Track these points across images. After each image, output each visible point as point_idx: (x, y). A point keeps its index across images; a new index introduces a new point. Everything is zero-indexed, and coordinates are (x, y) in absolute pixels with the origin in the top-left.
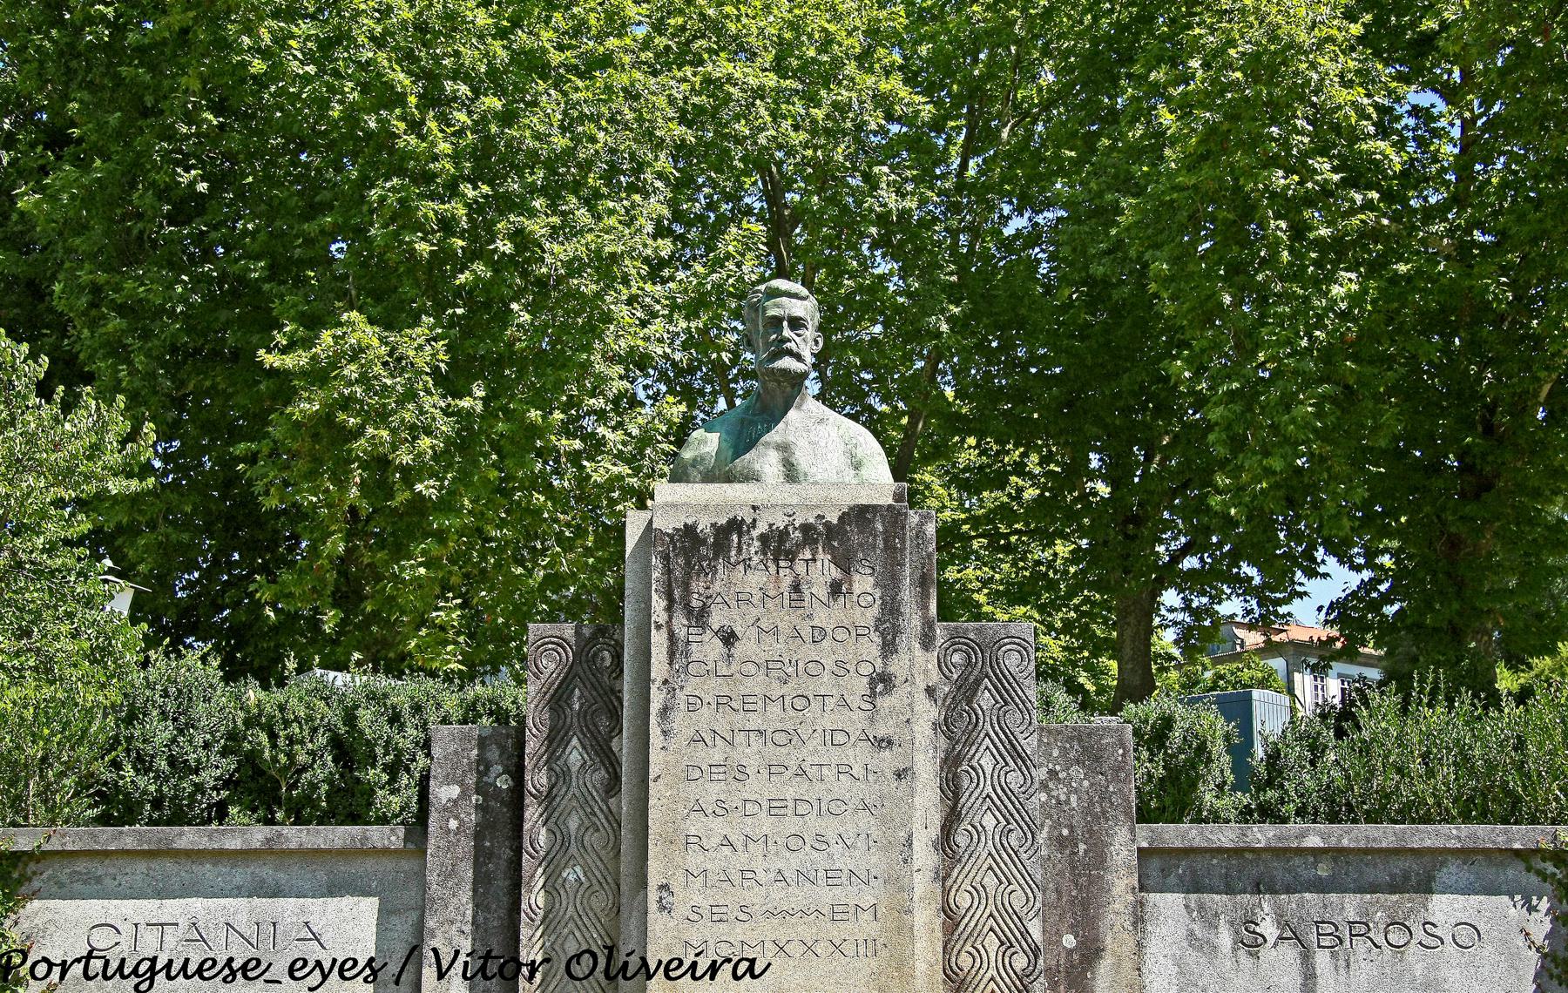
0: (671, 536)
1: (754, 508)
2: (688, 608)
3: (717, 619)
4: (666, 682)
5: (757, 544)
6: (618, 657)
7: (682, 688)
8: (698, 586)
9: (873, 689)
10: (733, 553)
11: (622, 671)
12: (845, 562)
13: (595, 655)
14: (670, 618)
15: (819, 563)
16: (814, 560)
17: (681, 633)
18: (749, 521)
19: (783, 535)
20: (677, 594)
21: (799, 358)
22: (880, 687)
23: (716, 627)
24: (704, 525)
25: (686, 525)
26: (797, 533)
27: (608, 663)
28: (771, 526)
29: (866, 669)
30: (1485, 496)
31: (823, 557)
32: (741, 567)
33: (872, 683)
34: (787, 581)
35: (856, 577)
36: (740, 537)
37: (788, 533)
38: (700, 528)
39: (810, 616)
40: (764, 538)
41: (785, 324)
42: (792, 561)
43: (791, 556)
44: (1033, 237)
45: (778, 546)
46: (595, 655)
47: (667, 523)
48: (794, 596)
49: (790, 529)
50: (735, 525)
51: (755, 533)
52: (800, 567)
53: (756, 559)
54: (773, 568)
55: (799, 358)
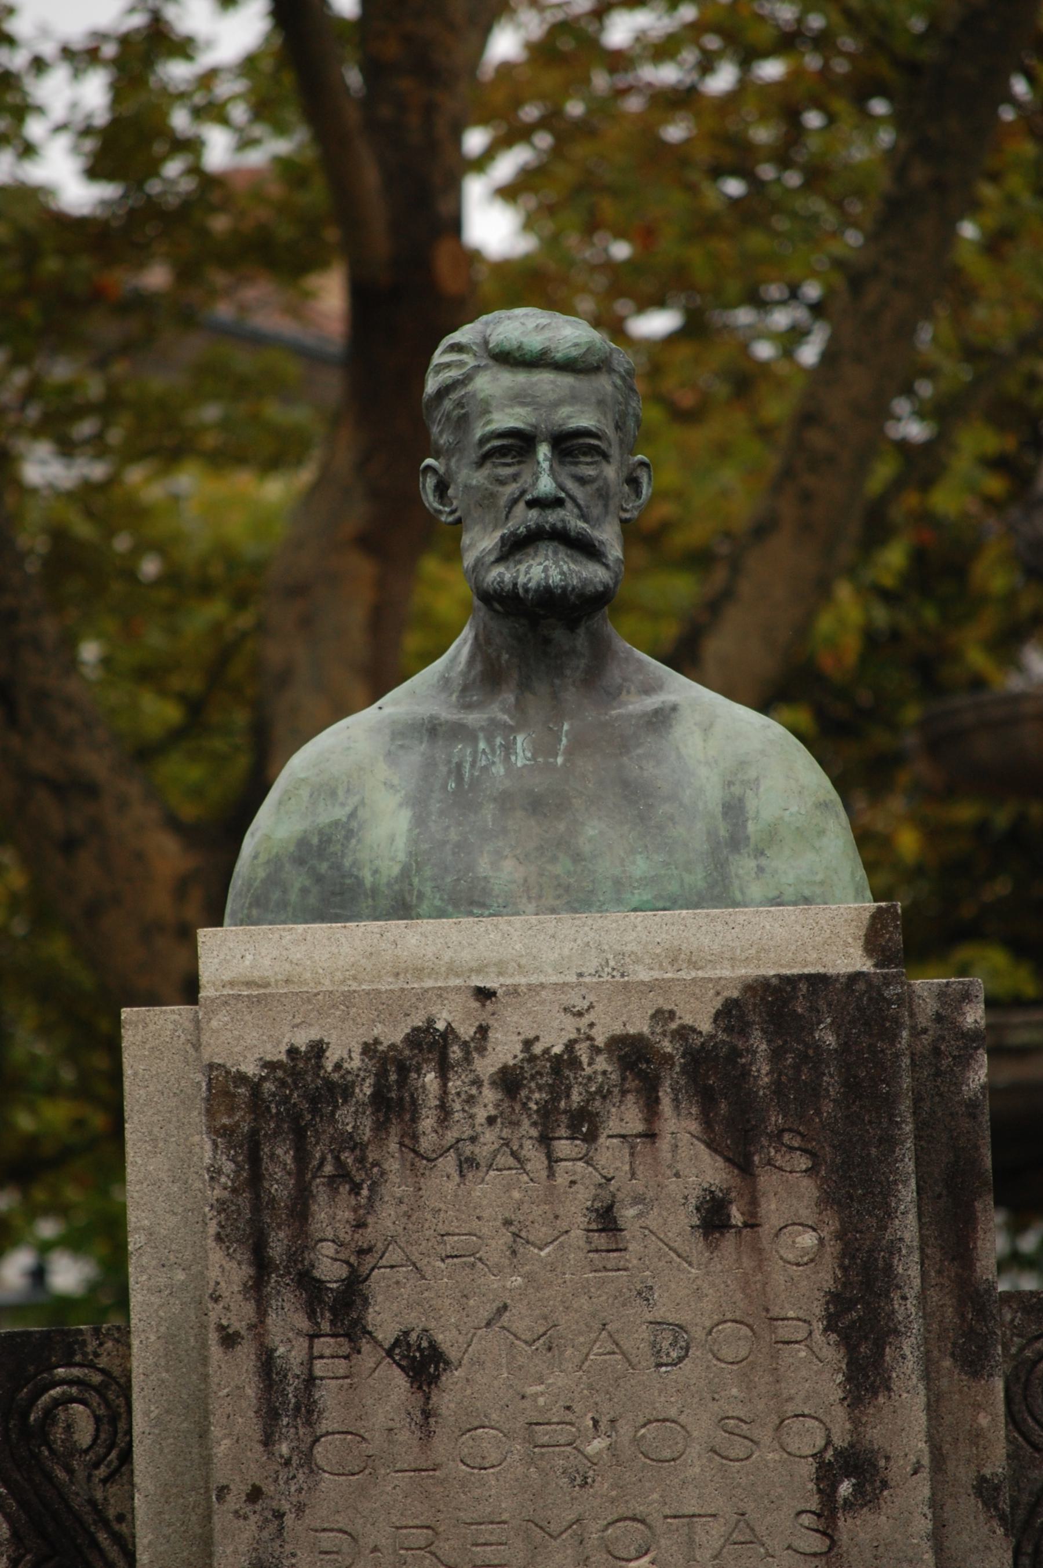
0: (255, 1087)
1: (484, 995)
2: (309, 1285)
3: (385, 1318)
4: (255, 1494)
5: (490, 1095)
6: (115, 1420)
7: (300, 1509)
8: (331, 1216)
9: (828, 1495)
10: (427, 1123)
11: (126, 1456)
12: (737, 1139)
13: (49, 1414)
14: (262, 1312)
15: (664, 1144)
16: (650, 1136)
17: (291, 1353)
18: (466, 1031)
19: (564, 1063)
20: (278, 1245)
21: (586, 548)
22: (845, 1488)
23: (387, 1334)
24: (344, 1049)
25: (293, 1052)
26: (602, 1063)
27: (84, 1435)
28: (528, 1044)
29: (807, 1439)
30: (365, 1246)
31: (680, 1126)
32: (448, 1163)
33: (827, 1475)
34: (576, 1208)
35: (767, 1180)
36: (444, 1078)
37: (575, 1063)
38: (332, 1057)
39: (645, 1294)
40: (509, 1082)
41: (543, 451)
42: (591, 1138)
43: (585, 1125)
44: (836, 234)
45: (550, 1097)
46: (49, 1414)
47: (250, 1046)
48: (601, 1240)
49: (582, 1052)
50: (432, 1044)
51: (487, 1066)
52: (610, 1154)
53: (490, 1136)
54: (537, 1160)
55: (586, 548)
